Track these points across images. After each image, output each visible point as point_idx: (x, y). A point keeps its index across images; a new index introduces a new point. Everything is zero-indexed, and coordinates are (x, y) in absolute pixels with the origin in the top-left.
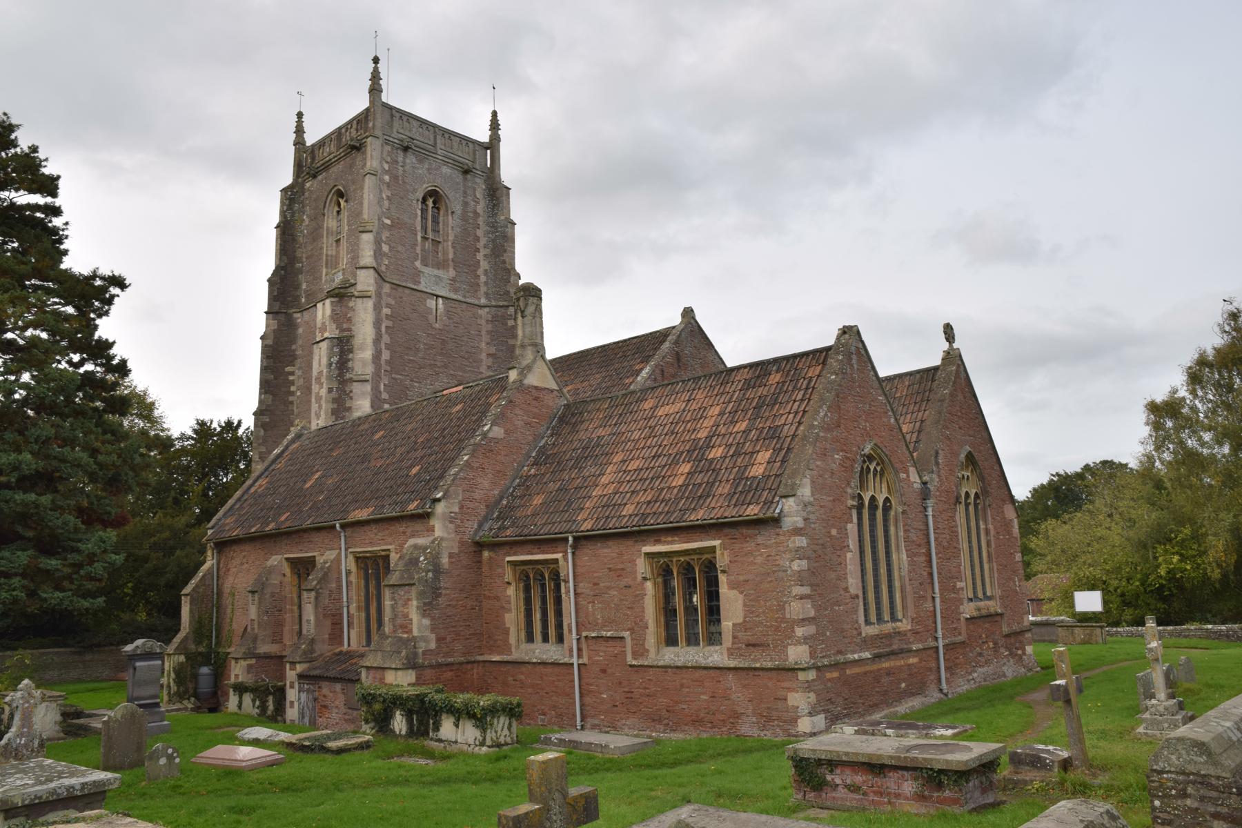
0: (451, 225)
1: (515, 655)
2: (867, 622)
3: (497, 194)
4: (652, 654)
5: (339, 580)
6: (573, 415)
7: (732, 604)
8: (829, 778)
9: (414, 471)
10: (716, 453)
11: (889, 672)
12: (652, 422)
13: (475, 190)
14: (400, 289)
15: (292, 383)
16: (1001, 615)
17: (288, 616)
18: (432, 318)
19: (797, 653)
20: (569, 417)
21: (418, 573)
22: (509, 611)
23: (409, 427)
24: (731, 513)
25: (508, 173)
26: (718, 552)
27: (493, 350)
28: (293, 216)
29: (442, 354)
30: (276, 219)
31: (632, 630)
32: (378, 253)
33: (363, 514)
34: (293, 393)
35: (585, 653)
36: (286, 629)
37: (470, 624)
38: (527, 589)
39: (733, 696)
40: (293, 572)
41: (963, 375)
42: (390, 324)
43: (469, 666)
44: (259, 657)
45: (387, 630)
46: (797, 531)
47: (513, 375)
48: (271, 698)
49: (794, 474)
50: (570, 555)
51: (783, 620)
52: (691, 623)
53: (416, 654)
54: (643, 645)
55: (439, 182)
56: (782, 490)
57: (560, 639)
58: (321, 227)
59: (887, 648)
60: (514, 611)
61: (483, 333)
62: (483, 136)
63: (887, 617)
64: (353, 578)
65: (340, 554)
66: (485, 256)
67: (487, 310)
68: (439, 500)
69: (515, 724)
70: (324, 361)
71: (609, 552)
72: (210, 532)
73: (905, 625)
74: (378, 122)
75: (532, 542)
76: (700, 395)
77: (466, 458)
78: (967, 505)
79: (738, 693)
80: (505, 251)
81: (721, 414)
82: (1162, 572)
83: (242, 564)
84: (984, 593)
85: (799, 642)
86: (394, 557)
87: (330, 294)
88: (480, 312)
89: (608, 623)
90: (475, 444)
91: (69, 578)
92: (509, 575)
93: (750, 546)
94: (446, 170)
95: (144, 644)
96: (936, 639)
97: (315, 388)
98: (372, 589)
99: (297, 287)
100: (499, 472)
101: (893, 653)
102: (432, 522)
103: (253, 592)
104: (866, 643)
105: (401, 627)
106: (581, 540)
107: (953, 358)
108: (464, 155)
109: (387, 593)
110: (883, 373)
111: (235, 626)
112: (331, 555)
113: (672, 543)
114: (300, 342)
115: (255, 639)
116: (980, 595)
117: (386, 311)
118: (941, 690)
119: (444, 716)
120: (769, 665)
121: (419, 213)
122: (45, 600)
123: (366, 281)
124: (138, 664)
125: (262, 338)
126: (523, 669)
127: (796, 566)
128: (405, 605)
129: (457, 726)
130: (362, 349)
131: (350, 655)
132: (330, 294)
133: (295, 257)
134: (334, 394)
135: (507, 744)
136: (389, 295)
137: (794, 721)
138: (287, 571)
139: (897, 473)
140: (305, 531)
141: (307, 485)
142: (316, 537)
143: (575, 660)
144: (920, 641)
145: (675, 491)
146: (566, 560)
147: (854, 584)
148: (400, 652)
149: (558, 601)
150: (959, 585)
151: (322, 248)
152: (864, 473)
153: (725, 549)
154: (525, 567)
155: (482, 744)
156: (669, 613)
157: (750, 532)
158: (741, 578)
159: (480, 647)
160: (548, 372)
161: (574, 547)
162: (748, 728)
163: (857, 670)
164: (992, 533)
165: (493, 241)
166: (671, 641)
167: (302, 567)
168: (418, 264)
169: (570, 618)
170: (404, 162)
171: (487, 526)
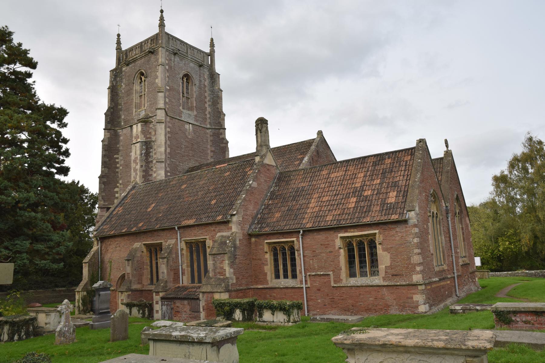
1: (270, 285)
3: (214, 77)
4: (344, 281)
5: (177, 253)
7: (384, 259)
8: (513, 319)
9: (213, 202)
10: (368, 193)
13: (204, 75)
14: (174, 120)
15: (118, 163)
16: (469, 264)
18: (187, 133)
19: (417, 278)
20: (283, 178)
21: (228, 248)
22: (267, 265)
23: (201, 183)
24: (384, 218)
25: (218, 68)
26: (377, 235)
27: (213, 149)
28: (116, 83)
29: (191, 150)
30: (108, 85)
31: (333, 271)
32: (165, 103)
33: (191, 222)
34: (118, 168)
35: (309, 282)
36: (144, 277)
37: (250, 270)
38: (275, 255)
39: (386, 298)
40: (147, 251)
42: (170, 135)
43: (248, 291)
44: (132, 291)
45: (211, 275)
46: (415, 226)
48: (147, 309)
49: (412, 201)
50: (300, 239)
51: (410, 264)
53: (228, 285)
54: (339, 277)
55: (189, 70)
56: (407, 208)
57: (294, 276)
58: (132, 89)
60: (269, 265)
61: (209, 141)
62: (207, 50)
64: (184, 252)
66: (209, 105)
67: (210, 130)
68: (234, 215)
69: (300, 312)
70: (138, 152)
71: (321, 237)
74: (162, 41)
75: (279, 233)
77: (244, 196)
79: (388, 297)
80: (218, 103)
81: (365, 176)
82: (501, 249)
83: (116, 247)
85: (418, 273)
86: (209, 243)
87: (140, 121)
88: (207, 131)
89: (321, 268)
90: (247, 190)
91: (47, 253)
92: (266, 248)
93: (393, 232)
94: (192, 65)
95: (103, 283)
96: (454, 273)
97: (133, 165)
98: (195, 257)
99: (119, 117)
100: (256, 202)
102: (230, 225)
103: (128, 260)
105: (219, 273)
106: (307, 232)
107: (448, 154)
108: (199, 58)
110: (433, 158)
111: (112, 277)
113: (353, 232)
114: (121, 143)
115: (130, 283)
117: (168, 129)
118: (456, 295)
119: (265, 311)
120: (404, 283)
121: (181, 84)
122: (37, 264)
123: (161, 115)
124: (101, 293)
125: (102, 141)
126: (275, 291)
129: (273, 314)
130: (159, 146)
131: (185, 288)
132: (140, 121)
133: (118, 103)
134: (144, 168)
135: (298, 321)
136: (169, 122)
137: (417, 307)
138: (144, 249)
140: (155, 231)
141: (149, 210)
145: (352, 210)
148: (221, 285)
151: (132, 99)
153: (381, 234)
154: (275, 245)
155: (289, 321)
157: (393, 226)
158: (389, 246)
159: (251, 282)
160: (272, 158)
162: (394, 311)
165: (213, 98)
166: (352, 275)
167: (154, 250)
168: (181, 108)
170: (174, 60)
171: (253, 227)
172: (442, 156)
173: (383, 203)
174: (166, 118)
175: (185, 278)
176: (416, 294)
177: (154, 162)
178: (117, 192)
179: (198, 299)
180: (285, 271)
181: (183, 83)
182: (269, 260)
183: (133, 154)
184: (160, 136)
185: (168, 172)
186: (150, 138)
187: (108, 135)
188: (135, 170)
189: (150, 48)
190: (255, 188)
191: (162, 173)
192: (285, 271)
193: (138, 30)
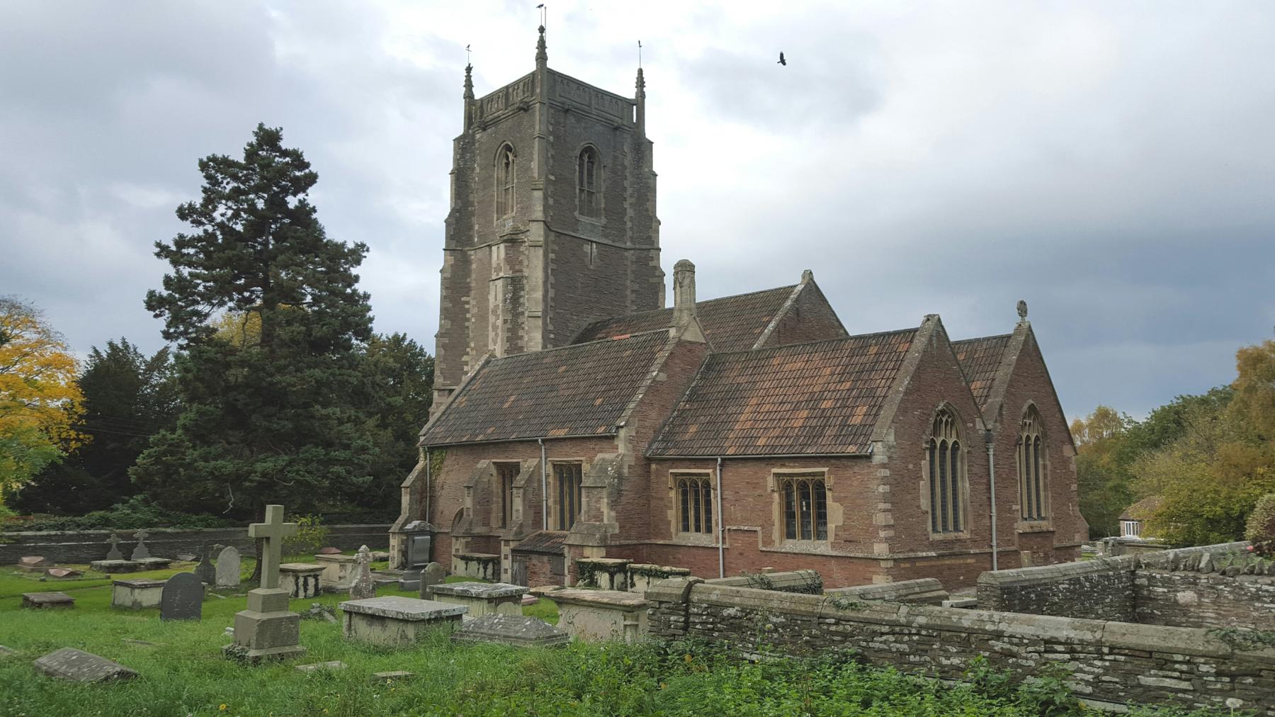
0: (602, 178)
1: (675, 541)
2: (935, 530)
4: (777, 543)
5: (540, 481)
6: (718, 364)
7: (835, 513)
9: (598, 402)
11: (950, 568)
12: (779, 376)
16: (1053, 532)
17: (494, 507)
18: (587, 260)
19: (880, 549)
22: (671, 508)
27: (636, 287)
33: (562, 433)
34: (468, 320)
36: (493, 515)
38: (685, 494)
40: (498, 473)
41: (1031, 342)
44: (473, 536)
46: (883, 466)
47: (672, 332)
51: (871, 525)
52: (805, 525)
53: (606, 537)
57: (709, 530)
59: (950, 550)
62: (629, 93)
63: (951, 527)
64: (551, 480)
65: (540, 462)
70: (500, 297)
71: (747, 471)
72: (422, 439)
73: (965, 535)
76: (816, 357)
78: (1027, 446)
81: (832, 374)
84: (1039, 515)
86: (586, 468)
89: (745, 520)
93: (849, 473)
94: (598, 128)
97: (492, 319)
98: (566, 488)
99: (471, 228)
101: (955, 554)
104: (933, 545)
109: (583, 491)
112: (532, 462)
114: (474, 276)
116: (1035, 516)
117: (552, 256)
120: (860, 555)
123: (536, 232)
127: (881, 489)
128: (598, 501)
130: (533, 289)
131: (549, 537)
138: (494, 472)
139: (964, 422)
140: (510, 442)
142: (520, 448)
143: (720, 545)
144: (977, 547)
146: (715, 472)
147: (925, 503)
149: (708, 503)
150: (1014, 507)
152: (937, 425)
156: (789, 515)
161: (721, 466)
163: (925, 564)
164: (1049, 467)
166: (791, 535)
167: (508, 472)
168: (576, 214)
169: (717, 515)
172: (1012, 332)
173: (843, 425)
174: (546, 236)
175: (551, 520)
176: (877, 573)
177: (526, 314)
178: (466, 363)
179: (562, 555)
180: (697, 520)
181: (581, 166)
182: (674, 501)
183: (491, 297)
184: (535, 270)
185: (551, 332)
186: (521, 271)
187: (451, 260)
188: (495, 328)
189: (521, 101)
190: (662, 383)
191: (538, 336)
192: (697, 520)
193: (502, 68)
